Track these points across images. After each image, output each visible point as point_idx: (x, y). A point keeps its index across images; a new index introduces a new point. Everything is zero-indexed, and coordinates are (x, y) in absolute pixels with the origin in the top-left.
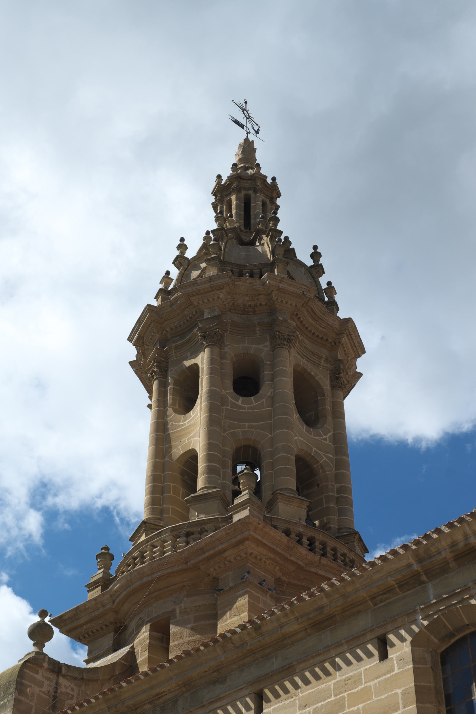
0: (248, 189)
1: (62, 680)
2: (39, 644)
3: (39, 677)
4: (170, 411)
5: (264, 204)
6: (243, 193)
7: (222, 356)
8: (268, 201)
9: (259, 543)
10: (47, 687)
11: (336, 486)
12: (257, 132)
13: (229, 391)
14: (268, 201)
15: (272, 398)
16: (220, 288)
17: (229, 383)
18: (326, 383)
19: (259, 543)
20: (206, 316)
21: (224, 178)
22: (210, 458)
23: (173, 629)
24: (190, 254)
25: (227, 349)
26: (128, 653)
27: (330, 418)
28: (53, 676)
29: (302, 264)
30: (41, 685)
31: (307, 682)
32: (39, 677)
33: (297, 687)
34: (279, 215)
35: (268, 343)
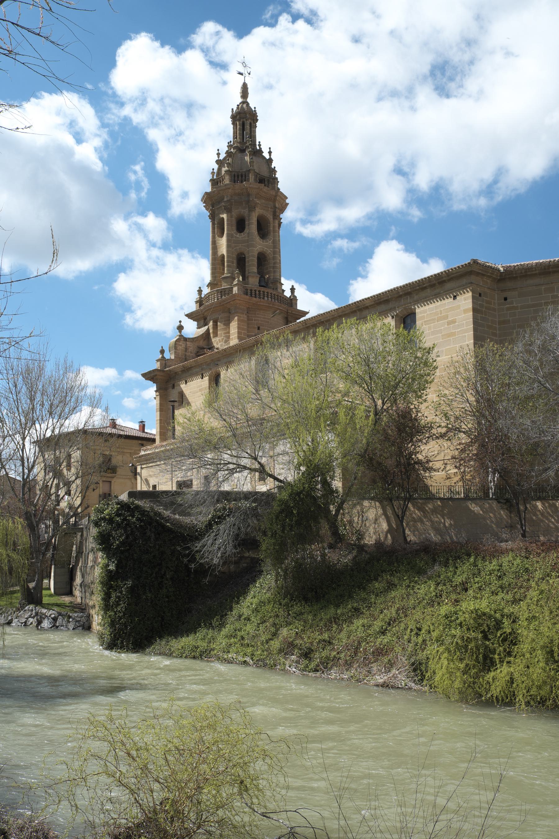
0: (244, 118)
1: (187, 343)
2: (180, 332)
3: (181, 343)
4: (216, 236)
5: (250, 124)
6: (242, 120)
7: (231, 217)
8: (252, 122)
9: (239, 300)
10: (183, 346)
11: (273, 261)
12: (249, 74)
13: (234, 231)
14: (252, 122)
15: (248, 233)
16: (229, 189)
17: (234, 228)
18: (271, 218)
19: (239, 300)
20: (225, 200)
21: (234, 110)
22: (228, 256)
23: (219, 324)
24: (221, 157)
25: (233, 213)
26: (206, 331)
27: (272, 233)
28: (185, 342)
29: (264, 158)
30: (181, 346)
31: (464, 293)
32: (181, 343)
33: (419, 307)
34: (258, 118)
35: (247, 209)
